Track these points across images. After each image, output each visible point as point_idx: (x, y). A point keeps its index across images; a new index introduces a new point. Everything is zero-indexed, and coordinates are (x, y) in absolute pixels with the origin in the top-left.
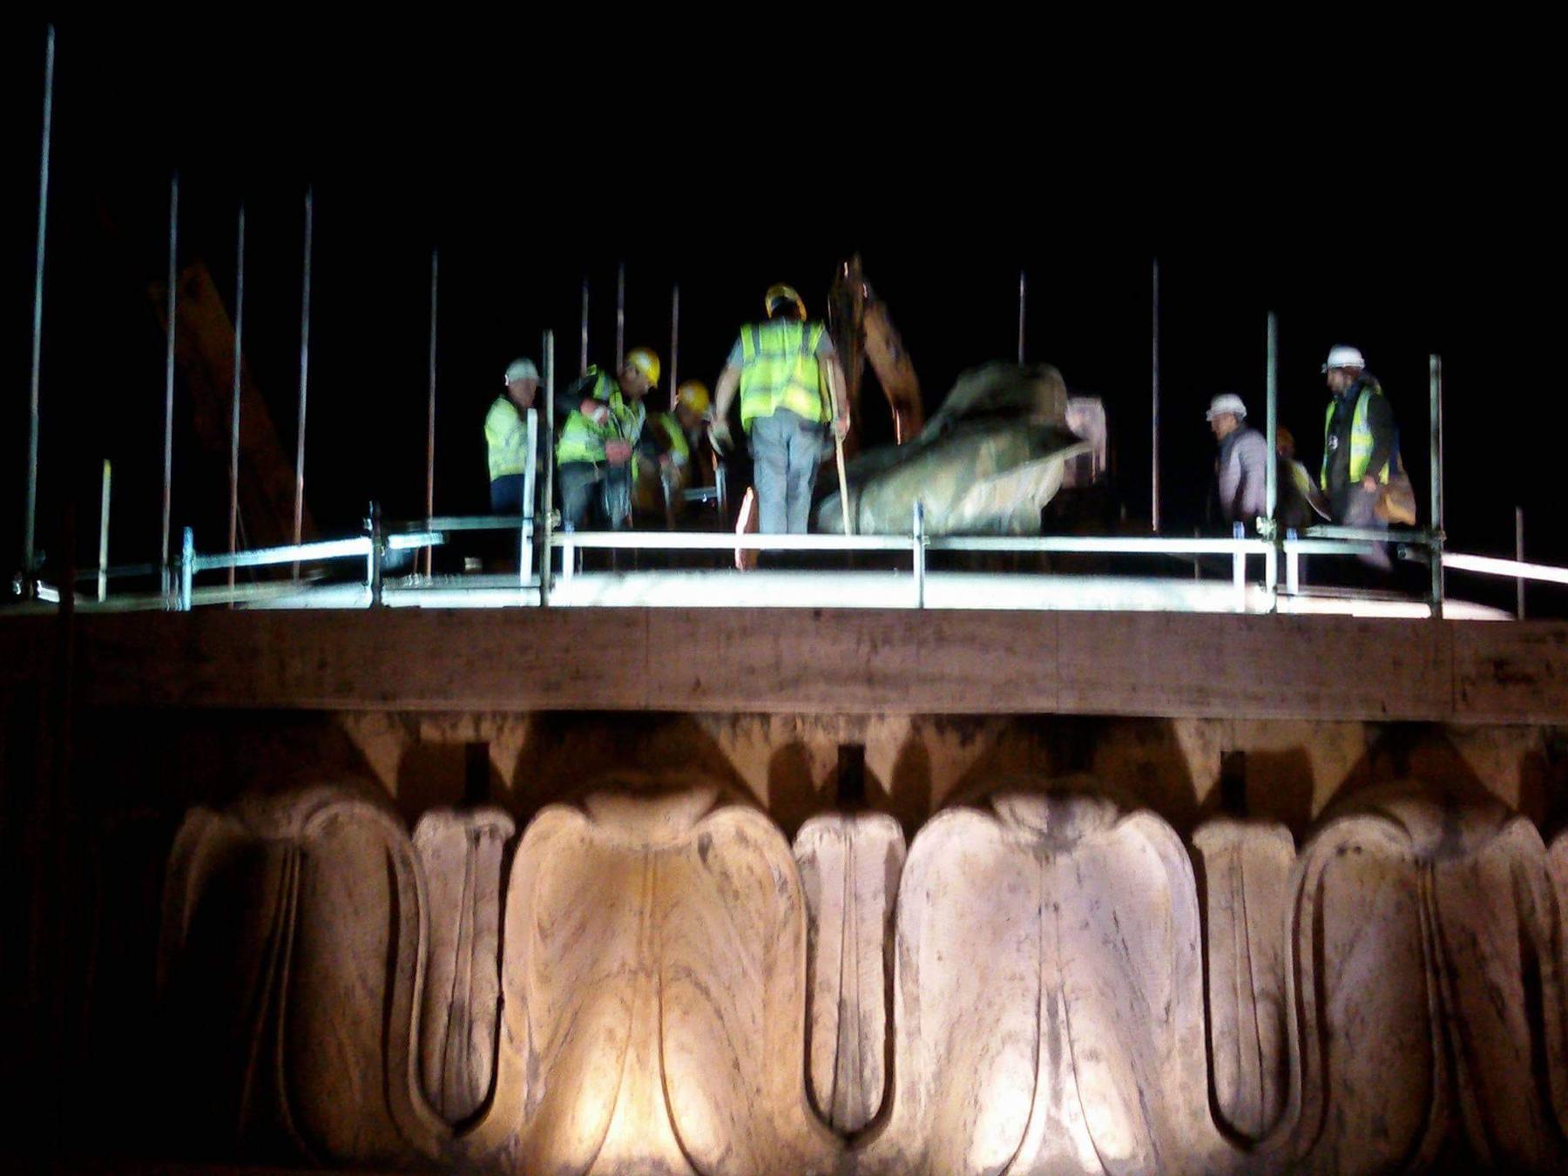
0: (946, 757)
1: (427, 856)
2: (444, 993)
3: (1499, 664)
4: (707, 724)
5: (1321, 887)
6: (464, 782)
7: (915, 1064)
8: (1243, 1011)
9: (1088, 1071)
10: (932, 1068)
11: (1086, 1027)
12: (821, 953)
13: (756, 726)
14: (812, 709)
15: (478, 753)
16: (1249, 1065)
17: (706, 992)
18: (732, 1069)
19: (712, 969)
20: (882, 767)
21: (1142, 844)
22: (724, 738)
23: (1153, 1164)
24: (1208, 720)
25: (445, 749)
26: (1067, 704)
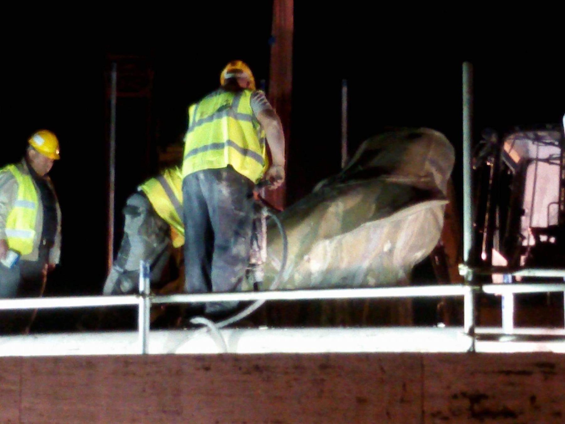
3: (476, 398)
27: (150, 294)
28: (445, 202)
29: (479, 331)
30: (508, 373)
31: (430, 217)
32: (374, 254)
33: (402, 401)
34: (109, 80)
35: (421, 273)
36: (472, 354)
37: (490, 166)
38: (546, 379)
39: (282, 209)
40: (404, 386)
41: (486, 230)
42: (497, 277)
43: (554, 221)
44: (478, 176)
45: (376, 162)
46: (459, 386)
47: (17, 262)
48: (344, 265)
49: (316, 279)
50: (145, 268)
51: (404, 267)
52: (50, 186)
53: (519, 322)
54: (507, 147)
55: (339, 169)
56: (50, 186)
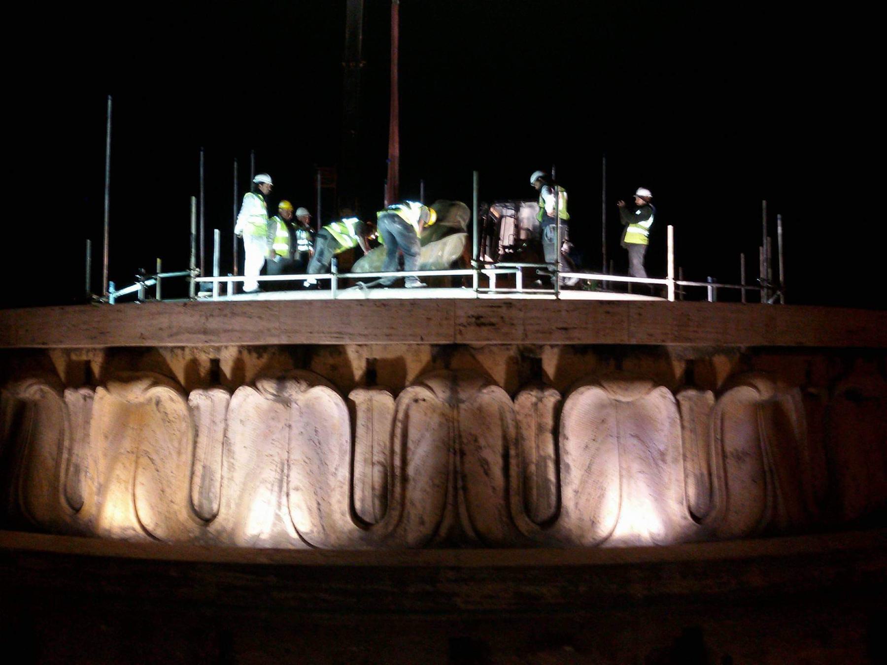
0: (252, 363)
1: (71, 406)
2: (74, 459)
3: (478, 318)
4: (162, 352)
5: (407, 416)
6: (85, 378)
7: (568, 494)
8: (368, 470)
9: (295, 497)
10: (238, 493)
11: (297, 477)
12: (199, 445)
13: (179, 352)
14: (200, 345)
15: (88, 363)
16: (368, 493)
17: (152, 460)
18: (161, 493)
19: (157, 452)
20: (227, 368)
21: (326, 398)
22: (168, 357)
23: (322, 536)
24: (360, 345)
25: (79, 363)
28: (465, 234)
30: (492, 307)
35: (455, 265)
36: (478, 299)
42: (487, 266)
43: (511, 243)
44: (480, 222)
46: (471, 313)
53: (497, 286)
54: (492, 210)
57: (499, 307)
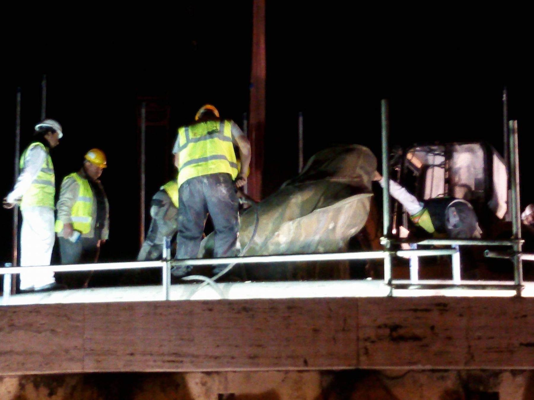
3: (395, 328)
24: (208, 373)
26: (90, 367)
27: (171, 260)
29: (395, 282)
30: (415, 310)
31: (360, 205)
32: (323, 230)
33: (344, 330)
34: (140, 114)
35: (354, 244)
36: (390, 298)
37: (397, 170)
38: (441, 314)
39: (259, 201)
40: (345, 320)
41: (396, 214)
42: (405, 246)
45: (323, 168)
46: (381, 321)
47: (79, 238)
48: (302, 239)
49: (283, 248)
50: (167, 242)
51: (343, 239)
52: (101, 187)
53: (422, 276)
54: (409, 156)
55: (298, 174)
56: (101, 187)
57: (427, 310)
